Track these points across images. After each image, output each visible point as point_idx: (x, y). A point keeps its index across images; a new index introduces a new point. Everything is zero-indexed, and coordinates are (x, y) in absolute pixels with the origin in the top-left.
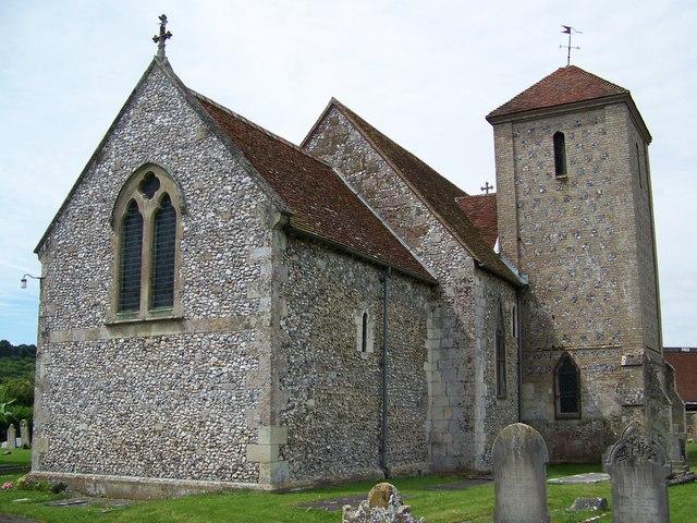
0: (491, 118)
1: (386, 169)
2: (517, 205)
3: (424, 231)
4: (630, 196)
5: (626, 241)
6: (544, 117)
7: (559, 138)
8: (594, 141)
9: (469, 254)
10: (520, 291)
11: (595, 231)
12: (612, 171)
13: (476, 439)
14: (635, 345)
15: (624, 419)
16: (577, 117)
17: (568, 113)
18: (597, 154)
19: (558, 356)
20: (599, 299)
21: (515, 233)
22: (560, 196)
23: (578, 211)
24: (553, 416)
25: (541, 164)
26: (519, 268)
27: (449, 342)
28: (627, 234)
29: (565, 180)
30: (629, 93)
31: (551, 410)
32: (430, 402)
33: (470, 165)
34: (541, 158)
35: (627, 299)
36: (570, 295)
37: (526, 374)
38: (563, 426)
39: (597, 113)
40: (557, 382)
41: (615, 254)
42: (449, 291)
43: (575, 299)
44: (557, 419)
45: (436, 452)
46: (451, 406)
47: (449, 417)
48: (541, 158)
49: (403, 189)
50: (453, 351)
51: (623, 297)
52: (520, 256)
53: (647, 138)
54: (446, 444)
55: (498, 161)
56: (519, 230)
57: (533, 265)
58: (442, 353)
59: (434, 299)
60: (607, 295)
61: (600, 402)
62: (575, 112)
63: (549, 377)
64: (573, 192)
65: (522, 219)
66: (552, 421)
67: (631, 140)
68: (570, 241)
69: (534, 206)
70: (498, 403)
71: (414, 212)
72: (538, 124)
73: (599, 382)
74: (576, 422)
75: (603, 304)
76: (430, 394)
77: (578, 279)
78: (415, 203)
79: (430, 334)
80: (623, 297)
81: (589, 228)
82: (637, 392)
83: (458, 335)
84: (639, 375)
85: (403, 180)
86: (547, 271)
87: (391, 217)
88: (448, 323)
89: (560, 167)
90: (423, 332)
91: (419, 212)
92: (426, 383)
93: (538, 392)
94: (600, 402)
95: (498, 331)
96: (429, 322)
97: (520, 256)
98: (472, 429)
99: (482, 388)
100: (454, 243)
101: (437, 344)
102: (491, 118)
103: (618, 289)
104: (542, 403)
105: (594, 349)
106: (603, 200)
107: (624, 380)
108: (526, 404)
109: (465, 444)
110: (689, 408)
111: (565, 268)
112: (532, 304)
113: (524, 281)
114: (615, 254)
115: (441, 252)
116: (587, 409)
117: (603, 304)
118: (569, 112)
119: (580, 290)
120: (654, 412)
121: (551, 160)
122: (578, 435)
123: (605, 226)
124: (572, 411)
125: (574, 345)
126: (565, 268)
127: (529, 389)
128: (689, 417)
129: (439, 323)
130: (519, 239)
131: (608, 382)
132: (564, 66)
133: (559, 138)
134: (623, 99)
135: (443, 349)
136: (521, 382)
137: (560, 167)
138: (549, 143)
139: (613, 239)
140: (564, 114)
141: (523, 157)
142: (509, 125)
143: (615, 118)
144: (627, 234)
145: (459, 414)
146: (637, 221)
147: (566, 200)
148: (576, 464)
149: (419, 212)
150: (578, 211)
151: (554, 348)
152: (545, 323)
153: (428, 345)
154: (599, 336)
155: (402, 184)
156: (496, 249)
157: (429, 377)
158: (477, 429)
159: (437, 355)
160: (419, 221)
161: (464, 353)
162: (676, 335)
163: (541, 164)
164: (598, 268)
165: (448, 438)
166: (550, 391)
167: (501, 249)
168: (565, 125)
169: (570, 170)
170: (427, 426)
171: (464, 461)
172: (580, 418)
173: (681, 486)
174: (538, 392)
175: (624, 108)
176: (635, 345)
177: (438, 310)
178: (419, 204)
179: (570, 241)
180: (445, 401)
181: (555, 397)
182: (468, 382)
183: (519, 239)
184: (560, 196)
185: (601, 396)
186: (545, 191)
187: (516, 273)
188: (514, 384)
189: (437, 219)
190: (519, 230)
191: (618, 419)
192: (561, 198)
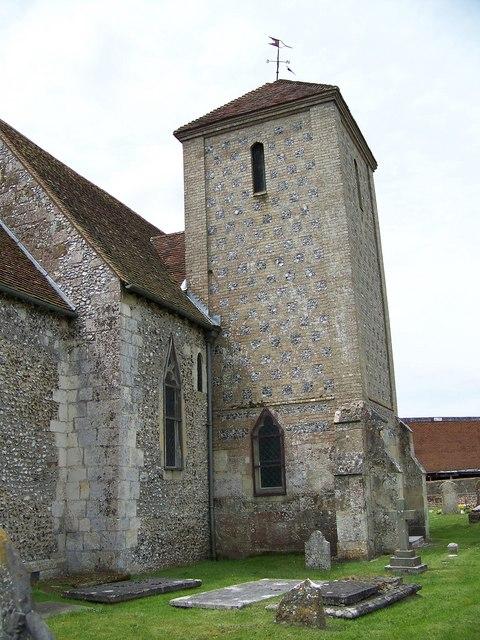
0: (182, 134)
1: (28, 179)
2: (209, 233)
3: (63, 249)
4: (342, 210)
5: (338, 264)
6: (240, 127)
7: (257, 150)
8: (303, 152)
9: (116, 275)
10: (209, 334)
11: (300, 256)
12: (319, 181)
13: (121, 525)
14: (352, 396)
15: (338, 493)
16: (277, 123)
17: (278, 129)
18: (301, 164)
19: (256, 414)
20: (306, 340)
21: (205, 265)
22: (258, 216)
23: (279, 234)
24: (251, 492)
25: (236, 182)
26: (210, 306)
27: (87, 393)
28: (338, 256)
29: (264, 198)
30: (338, 90)
31: (248, 484)
32: (63, 474)
33: (155, 189)
34: (236, 174)
35: (341, 337)
36: (271, 337)
37: (216, 436)
38: (264, 504)
39: (302, 116)
40: (256, 448)
41: (324, 282)
42: (89, 325)
43: (277, 342)
44: (256, 495)
45: (70, 544)
46: (89, 482)
47: (86, 496)
48: (236, 174)
49: (43, 201)
50: (92, 406)
51: (336, 335)
52: (211, 292)
53: (372, 164)
54: (83, 533)
55: (187, 181)
56: (209, 261)
57: (226, 303)
58: (80, 409)
59: (72, 336)
60: (317, 334)
61: (310, 473)
62: (275, 118)
63: (246, 441)
64: (273, 211)
65: (214, 248)
66: (250, 498)
67: (340, 145)
68: (271, 270)
69: (228, 232)
70: (167, 476)
71: (54, 227)
72: (233, 136)
73: (308, 446)
74: (280, 498)
75: (311, 345)
76: (62, 463)
77: (281, 316)
78: (57, 216)
79: (63, 382)
80: (336, 335)
81: (293, 252)
82: (355, 454)
83: (99, 383)
84: (356, 435)
85: (44, 190)
86: (243, 308)
87: (27, 237)
88: (88, 367)
89: (259, 183)
90: (52, 380)
91: (60, 227)
92: (54, 449)
93: (233, 461)
94: (310, 473)
95: (168, 380)
96: (63, 367)
97: (211, 292)
98: (114, 512)
99: (132, 455)
100: (98, 261)
101: (73, 397)
102: (182, 134)
103: (329, 326)
104: (238, 476)
105: (302, 404)
106: (309, 217)
107: (338, 441)
108: (218, 477)
109: (105, 533)
110: (432, 476)
111: (264, 303)
112: (225, 351)
113: (215, 322)
114: (324, 282)
115: (83, 275)
116: (294, 481)
117: (311, 345)
118: (268, 119)
119: (284, 330)
120: (378, 482)
121: (248, 176)
122: (281, 516)
123: (312, 248)
124: (275, 485)
125: (276, 399)
126: (264, 303)
127: (222, 458)
128: (431, 489)
129: (77, 369)
130: (210, 272)
131: (319, 446)
132: (272, 80)
133: (257, 150)
134: (331, 96)
135: (81, 402)
136: (211, 447)
137: (259, 183)
138: (246, 157)
139: (323, 261)
140: (262, 121)
141: (216, 174)
142: (200, 140)
143: (321, 119)
144: (338, 256)
145: (98, 492)
146: (350, 240)
147: (266, 221)
148: (281, 554)
149: (60, 227)
150: (279, 234)
151: (252, 406)
152: (240, 374)
153: (58, 397)
154: (308, 388)
155: (43, 194)
156: (183, 287)
157: (60, 441)
158: (121, 511)
159: (73, 411)
160: (61, 237)
161: (105, 407)
162: (425, 390)
163: (236, 182)
164: (305, 301)
165: (84, 525)
166: (248, 460)
167: (188, 285)
168: (264, 133)
169: (271, 185)
170: (56, 509)
171: (105, 559)
172: (284, 494)
173: (387, 611)
174: (233, 461)
175: (332, 108)
176: (352, 396)
177: (76, 350)
178: (60, 217)
179: (271, 270)
180: (80, 474)
181: (254, 467)
182: (110, 448)
183: (210, 272)
184: (258, 216)
185: (309, 466)
186: (241, 212)
187: (206, 312)
188: (201, 452)
189: (79, 233)
190: (209, 261)
191: (330, 493)
192: (260, 219)
